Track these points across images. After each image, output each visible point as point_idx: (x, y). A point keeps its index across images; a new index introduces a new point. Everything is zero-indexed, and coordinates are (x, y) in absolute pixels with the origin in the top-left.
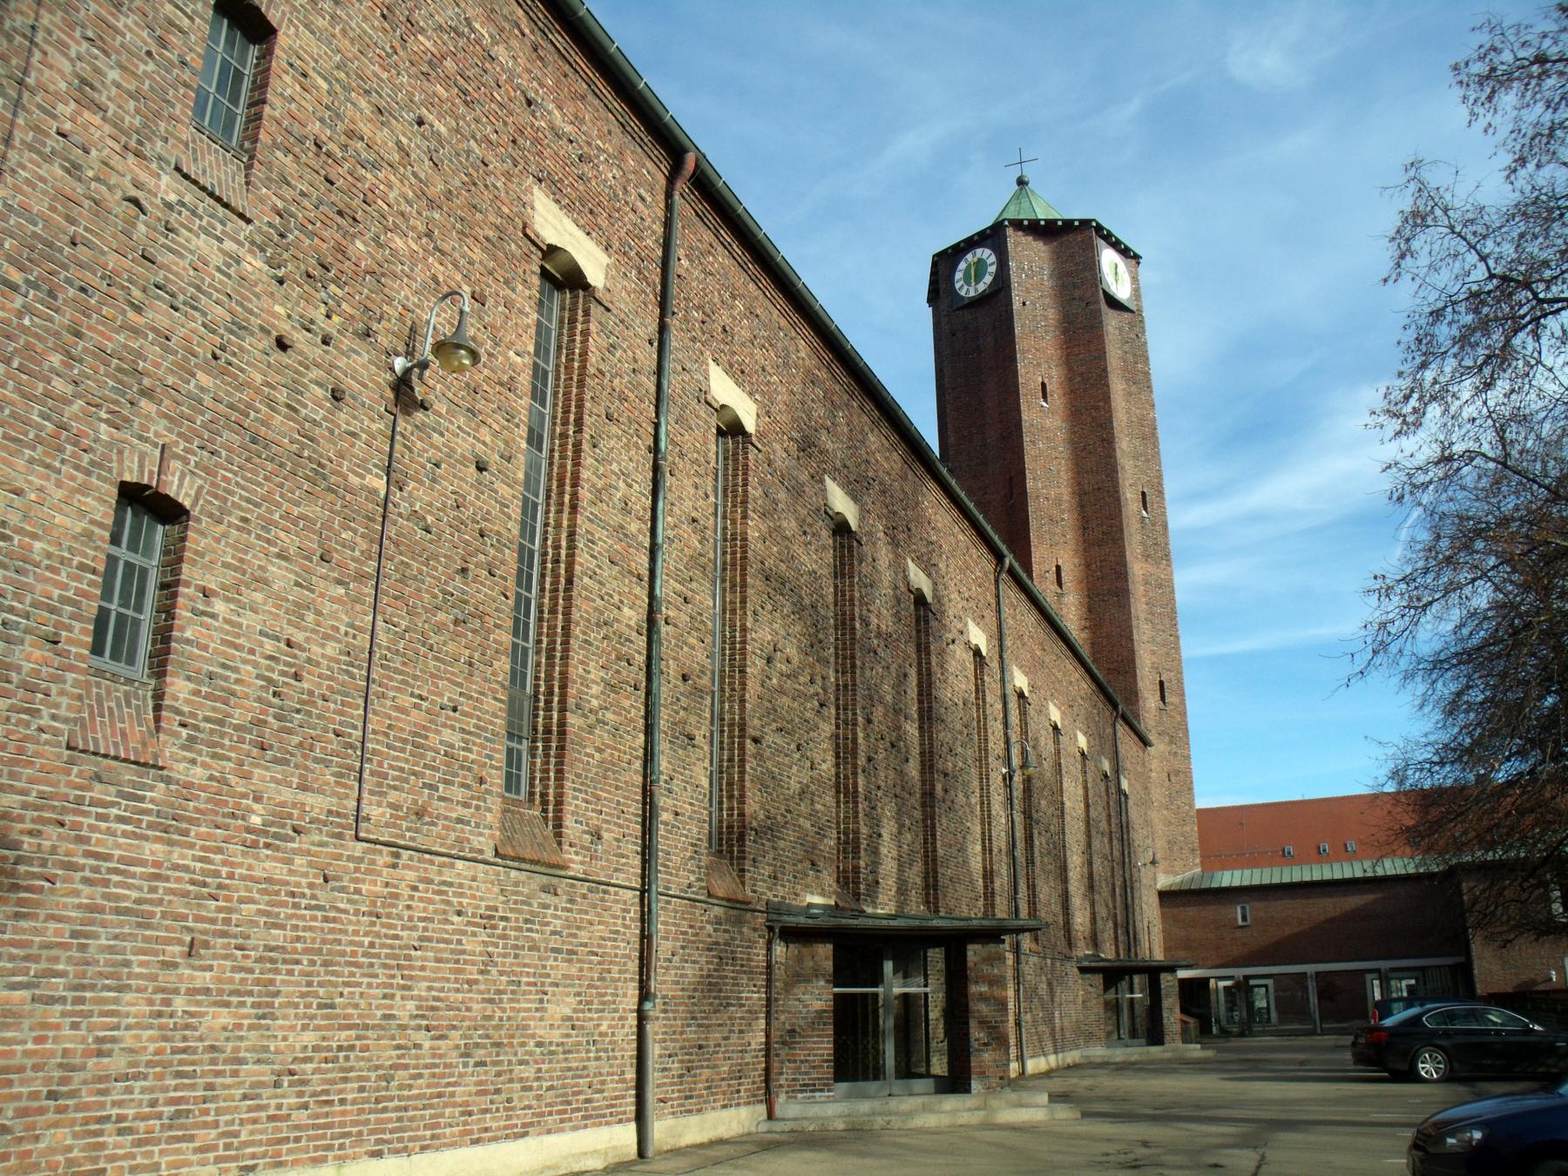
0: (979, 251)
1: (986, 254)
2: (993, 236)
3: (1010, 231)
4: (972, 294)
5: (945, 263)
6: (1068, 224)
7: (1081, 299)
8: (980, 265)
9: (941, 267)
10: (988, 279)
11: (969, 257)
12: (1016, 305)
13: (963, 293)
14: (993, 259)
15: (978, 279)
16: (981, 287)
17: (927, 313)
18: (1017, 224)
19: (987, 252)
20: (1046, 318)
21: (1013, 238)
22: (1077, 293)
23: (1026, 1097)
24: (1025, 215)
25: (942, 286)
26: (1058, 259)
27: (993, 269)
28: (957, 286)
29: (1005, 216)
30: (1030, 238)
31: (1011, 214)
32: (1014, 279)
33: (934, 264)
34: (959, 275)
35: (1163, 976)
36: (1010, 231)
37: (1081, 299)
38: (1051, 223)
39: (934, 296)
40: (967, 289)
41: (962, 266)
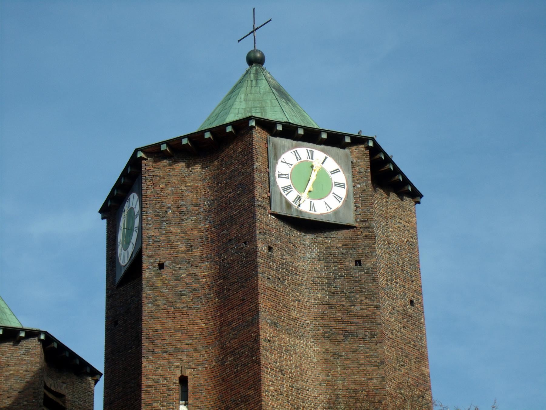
30: (181, 165)
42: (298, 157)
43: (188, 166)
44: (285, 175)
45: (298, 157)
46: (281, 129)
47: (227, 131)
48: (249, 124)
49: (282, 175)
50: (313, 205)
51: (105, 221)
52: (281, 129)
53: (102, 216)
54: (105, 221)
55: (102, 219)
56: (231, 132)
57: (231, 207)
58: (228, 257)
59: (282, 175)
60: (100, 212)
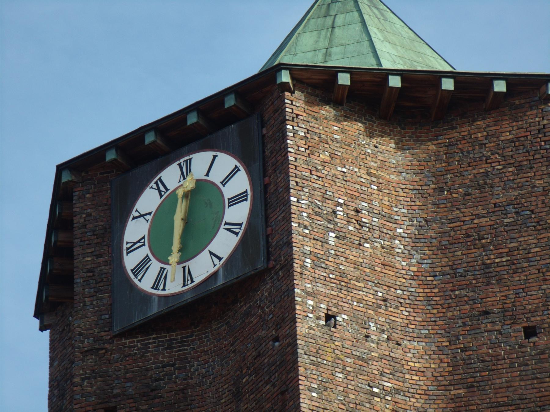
0: (200, 160)
1: (220, 168)
2: (244, 117)
3: (295, 103)
4: (174, 286)
5: (94, 189)
6: (474, 90)
7: (509, 315)
8: (204, 199)
9: (82, 208)
10: (224, 243)
11: (171, 175)
12: (308, 326)
13: (146, 284)
14: (241, 183)
15: (194, 240)
16: (202, 267)
17: (35, 346)
18: (319, 84)
19: (226, 162)
20: (396, 367)
21: (306, 124)
22: (495, 296)
23: (323, 159)
24: (345, 55)
25: (84, 259)
26: (437, 189)
27: (239, 213)
28: (130, 261)
29: (285, 58)
30: (356, 128)
31: (306, 53)
32: (303, 244)
33: (62, 195)
34: (135, 230)
35: (390, 77)
36: (295, 103)
37: (509, 315)
38: (420, 83)
39: (54, 300)
40: (160, 261)
41: (148, 201)
42: (236, 200)
43: (371, 135)
44: (139, 241)
45: (236, 200)
46: (399, 85)
47: (189, 123)
48: (224, 106)
49: (135, 244)
50: (189, 272)
51: (47, 333)
52: (399, 85)
53: (41, 323)
54: (47, 333)
55: (42, 329)
56: (154, 143)
57: (483, 246)
58: (479, 347)
59: (135, 244)
60: (36, 316)
